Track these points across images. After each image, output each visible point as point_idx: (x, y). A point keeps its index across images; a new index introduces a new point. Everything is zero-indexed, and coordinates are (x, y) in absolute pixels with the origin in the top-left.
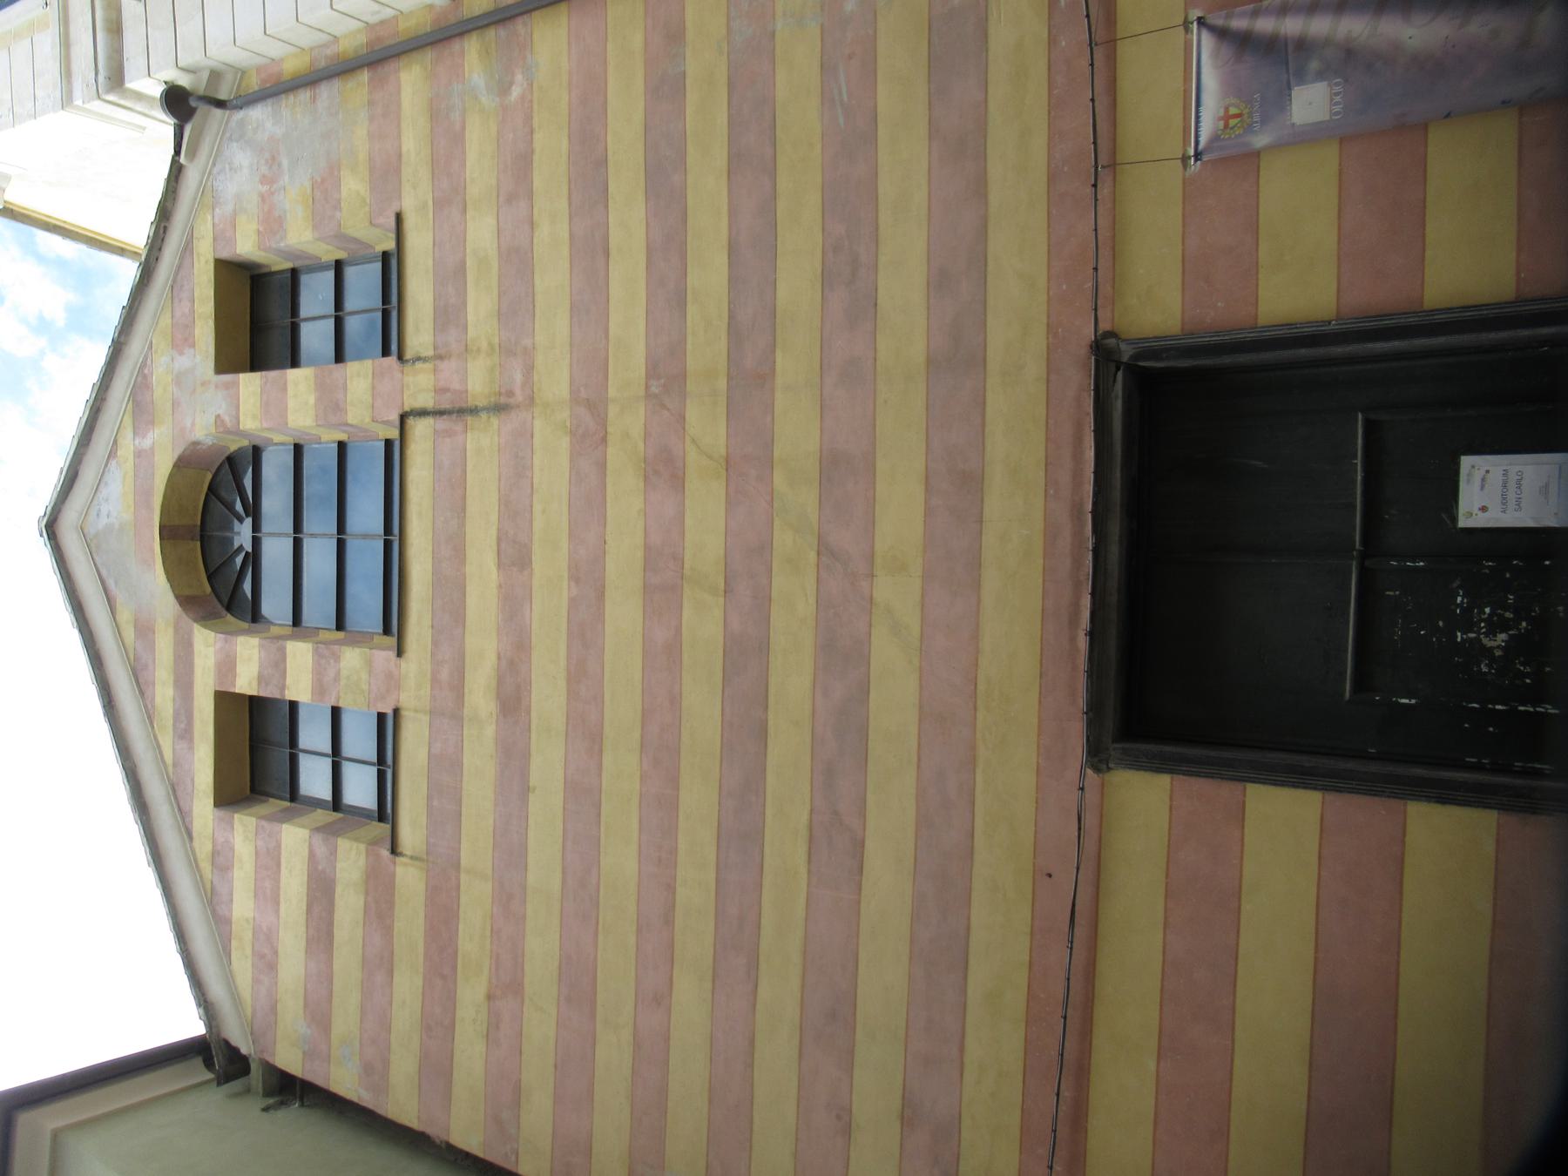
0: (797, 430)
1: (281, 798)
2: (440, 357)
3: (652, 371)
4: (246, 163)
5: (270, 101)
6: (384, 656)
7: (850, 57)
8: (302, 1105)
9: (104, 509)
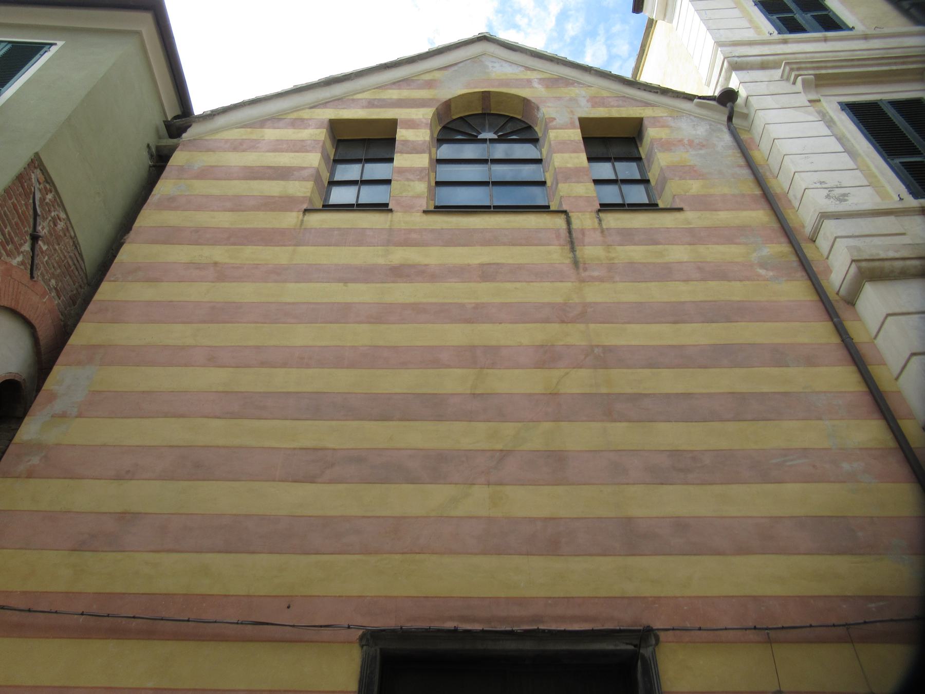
0: (580, 436)
1: (335, 155)
2: (602, 231)
3: (608, 349)
4: (699, 132)
5: (735, 144)
6: (423, 204)
7: (814, 466)
8: (150, 166)
9: (496, 65)
